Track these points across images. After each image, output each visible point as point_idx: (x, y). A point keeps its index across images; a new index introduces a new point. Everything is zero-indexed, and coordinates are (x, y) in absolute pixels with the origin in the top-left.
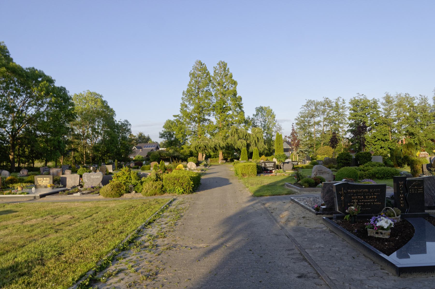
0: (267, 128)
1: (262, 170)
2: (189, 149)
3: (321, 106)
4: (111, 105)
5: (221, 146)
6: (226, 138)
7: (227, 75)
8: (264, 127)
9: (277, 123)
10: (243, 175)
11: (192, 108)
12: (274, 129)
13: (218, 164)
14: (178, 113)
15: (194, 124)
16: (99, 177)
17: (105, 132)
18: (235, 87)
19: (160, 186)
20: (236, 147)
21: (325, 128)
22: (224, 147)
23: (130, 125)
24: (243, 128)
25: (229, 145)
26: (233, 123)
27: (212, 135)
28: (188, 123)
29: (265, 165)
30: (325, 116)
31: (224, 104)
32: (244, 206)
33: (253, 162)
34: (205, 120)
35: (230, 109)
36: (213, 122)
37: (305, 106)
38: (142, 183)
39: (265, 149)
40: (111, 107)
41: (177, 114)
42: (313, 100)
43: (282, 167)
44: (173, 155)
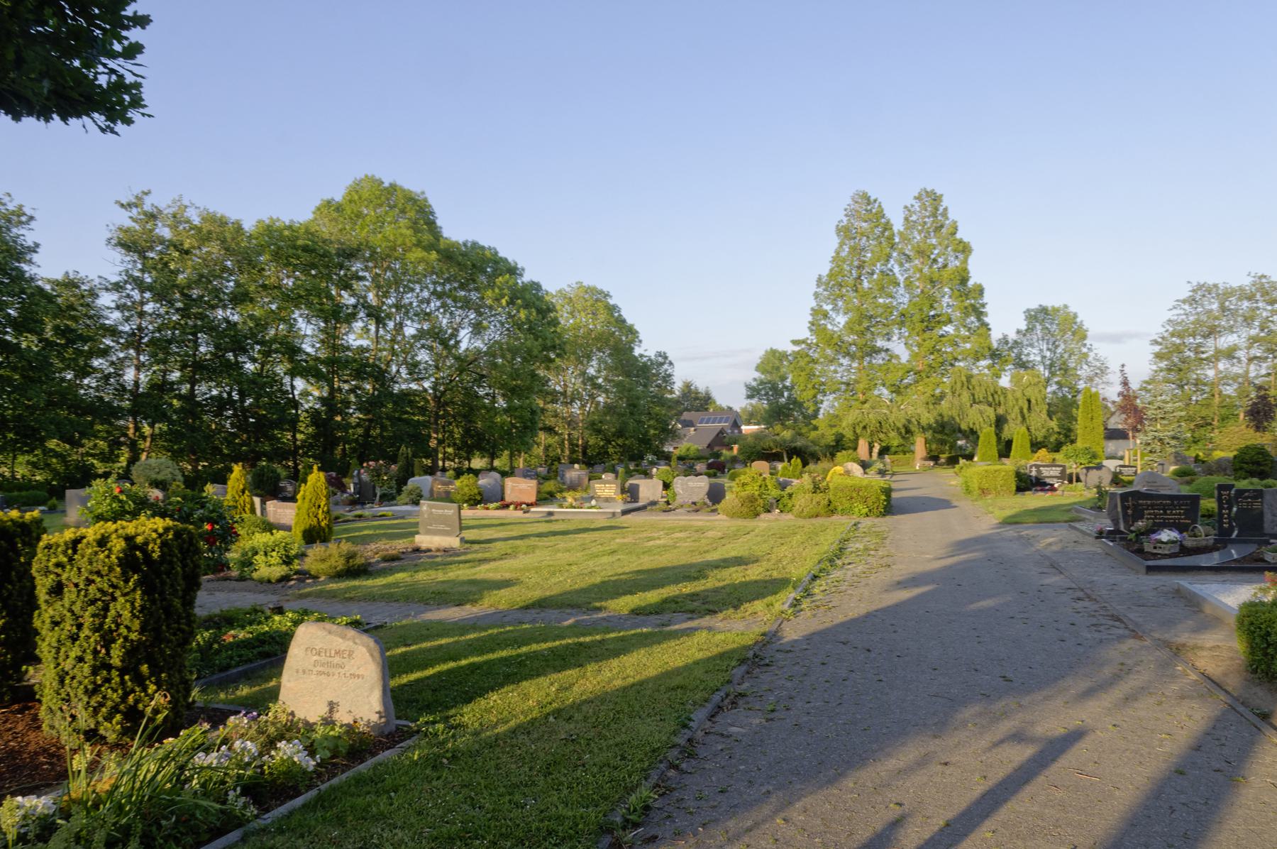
0: (1060, 368)
1: (1026, 483)
2: (834, 430)
3: (1240, 299)
4: (630, 318)
5: (924, 422)
6: (938, 399)
7: (942, 226)
8: (1051, 365)
9: (1092, 355)
10: (984, 492)
11: (841, 320)
12: (1084, 371)
13: (912, 470)
14: (804, 333)
15: (845, 361)
16: (702, 484)
17: (618, 384)
18: (965, 261)
19: (826, 502)
20: (964, 426)
21: (1252, 367)
22: (930, 427)
23: (671, 363)
24: (986, 371)
25: (946, 419)
26: (956, 359)
27: (897, 390)
28: (832, 361)
29: (1039, 472)
30: (1253, 332)
31: (932, 307)
32: (983, 533)
33: (1009, 465)
34: (878, 351)
35: (950, 321)
36: (898, 357)
37: (1184, 302)
38: (790, 495)
39: (1050, 432)
40: (629, 321)
41: (801, 338)
42: (1211, 282)
43: (1082, 477)
44: (793, 445)
